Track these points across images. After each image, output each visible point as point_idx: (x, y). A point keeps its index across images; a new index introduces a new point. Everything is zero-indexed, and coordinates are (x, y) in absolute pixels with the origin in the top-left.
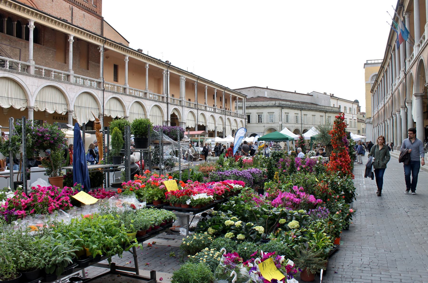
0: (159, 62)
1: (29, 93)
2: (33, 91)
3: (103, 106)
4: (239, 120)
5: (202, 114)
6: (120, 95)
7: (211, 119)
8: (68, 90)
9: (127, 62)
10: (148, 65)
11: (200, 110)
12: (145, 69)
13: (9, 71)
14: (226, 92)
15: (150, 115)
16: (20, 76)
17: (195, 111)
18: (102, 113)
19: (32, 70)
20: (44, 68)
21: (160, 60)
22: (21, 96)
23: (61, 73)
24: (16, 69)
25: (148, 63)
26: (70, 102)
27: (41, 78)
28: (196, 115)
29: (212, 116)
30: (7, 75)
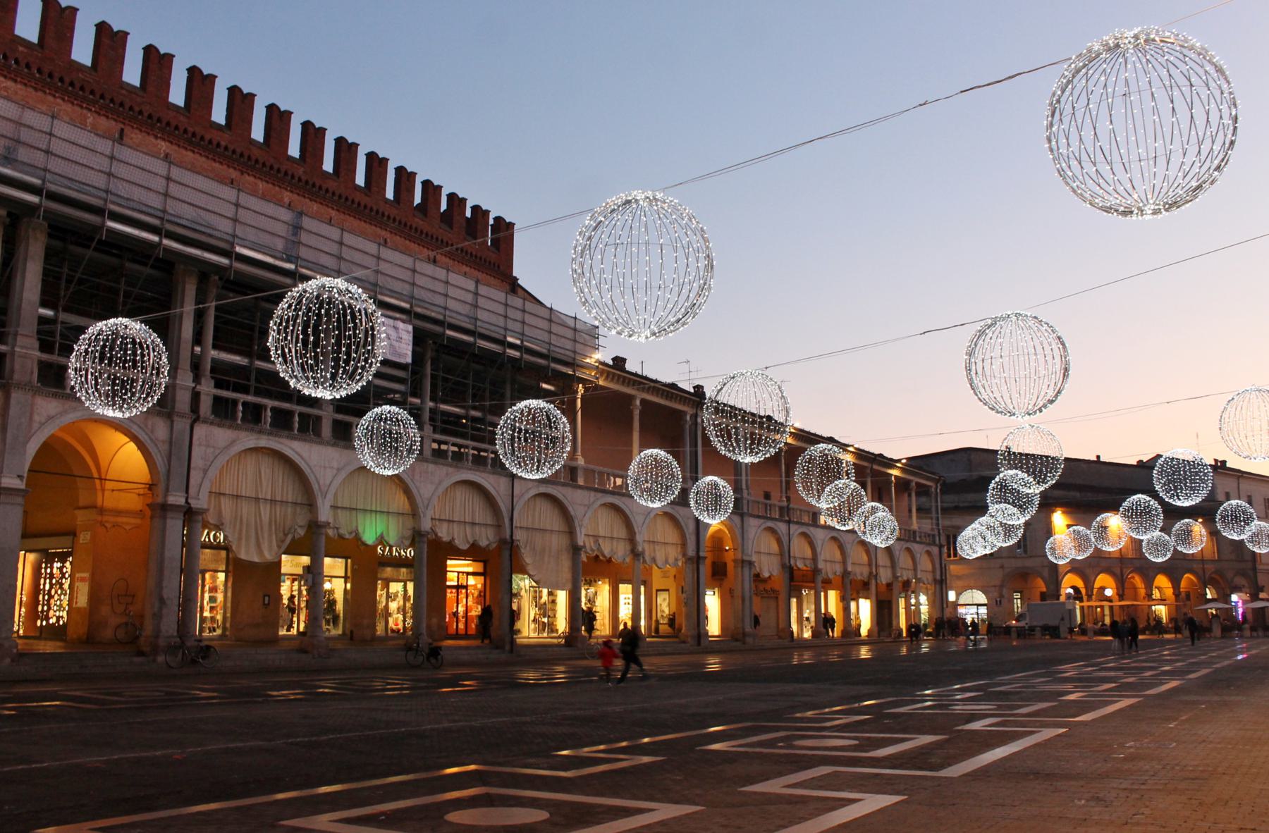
0: (672, 390)
1: (315, 487)
2: (328, 482)
3: (512, 519)
4: (916, 548)
5: (804, 535)
6: (560, 488)
7: (547, 517)
8: (417, 477)
9: (637, 413)
10: (638, 402)
11: (797, 523)
12: (631, 412)
13: (270, 434)
14: (875, 467)
15: (825, 561)
16: (296, 445)
17: (781, 527)
18: (508, 537)
19: (326, 430)
20: (270, 403)
21: (673, 386)
22: (621, 532)
23: (467, 447)
24: (318, 433)
25: (640, 396)
26: (421, 509)
27: (322, 443)
28: (504, 506)
29: (908, 549)
30: (264, 442)
